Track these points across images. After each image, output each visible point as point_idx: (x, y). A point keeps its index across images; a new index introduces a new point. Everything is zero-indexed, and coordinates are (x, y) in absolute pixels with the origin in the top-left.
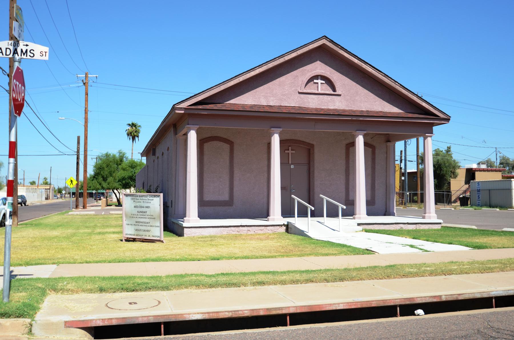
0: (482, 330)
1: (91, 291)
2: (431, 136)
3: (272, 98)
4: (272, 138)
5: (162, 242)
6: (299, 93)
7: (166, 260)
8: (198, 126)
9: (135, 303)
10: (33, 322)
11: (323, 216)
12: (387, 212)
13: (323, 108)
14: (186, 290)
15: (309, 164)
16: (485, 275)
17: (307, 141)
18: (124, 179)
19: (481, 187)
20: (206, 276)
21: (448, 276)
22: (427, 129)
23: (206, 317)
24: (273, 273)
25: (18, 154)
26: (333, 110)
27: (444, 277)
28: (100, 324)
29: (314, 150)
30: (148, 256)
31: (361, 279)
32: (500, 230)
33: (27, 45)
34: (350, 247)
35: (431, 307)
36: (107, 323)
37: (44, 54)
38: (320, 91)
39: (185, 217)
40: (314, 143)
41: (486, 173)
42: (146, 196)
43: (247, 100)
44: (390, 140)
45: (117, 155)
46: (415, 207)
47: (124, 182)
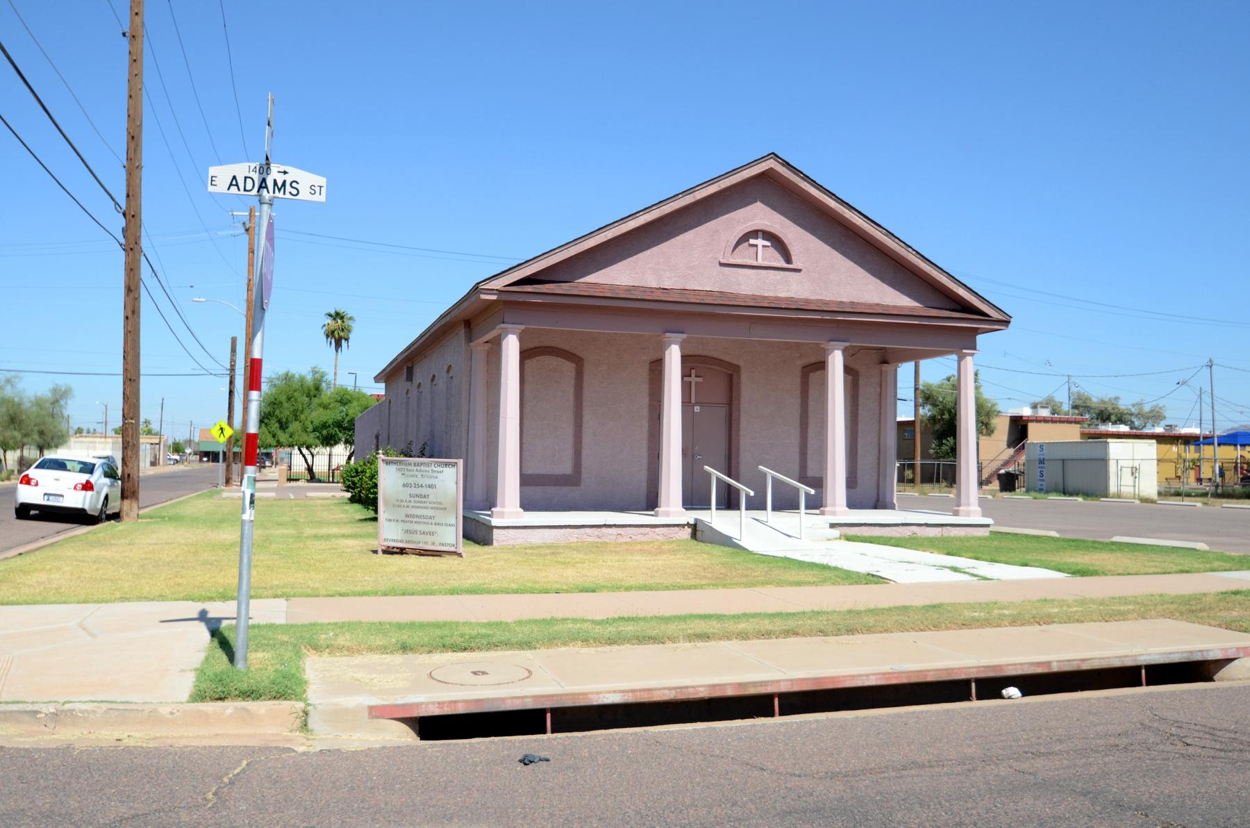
0: (1146, 722)
1: (384, 650)
2: (972, 355)
3: (668, 274)
4: (667, 352)
5: (460, 555)
6: (722, 264)
7: (495, 592)
8: (523, 327)
9: (484, 673)
10: (309, 708)
11: (764, 508)
12: (880, 503)
13: (766, 295)
14: (563, 649)
15: (730, 404)
16: (1113, 626)
17: (727, 359)
18: (325, 426)
19: (1047, 454)
20: (593, 622)
21: (1044, 627)
22: (964, 341)
23: (629, 698)
24: (720, 617)
25: (142, 372)
26: (787, 298)
27: (1037, 627)
28: (436, 711)
29: (739, 378)
30: (456, 584)
31: (886, 631)
32: (1106, 540)
33: (285, 173)
34: (836, 569)
35: (1034, 684)
36: (447, 711)
37: (317, 189)
38: (760, 262)
39: (495, 506)
40: (740, 363)
41: (1050, 425)
42: (428, 465)
43: (619, 276)
44: (887, 359)
45: (309, 378)
46: (935, 492)
47: (325, 432)
